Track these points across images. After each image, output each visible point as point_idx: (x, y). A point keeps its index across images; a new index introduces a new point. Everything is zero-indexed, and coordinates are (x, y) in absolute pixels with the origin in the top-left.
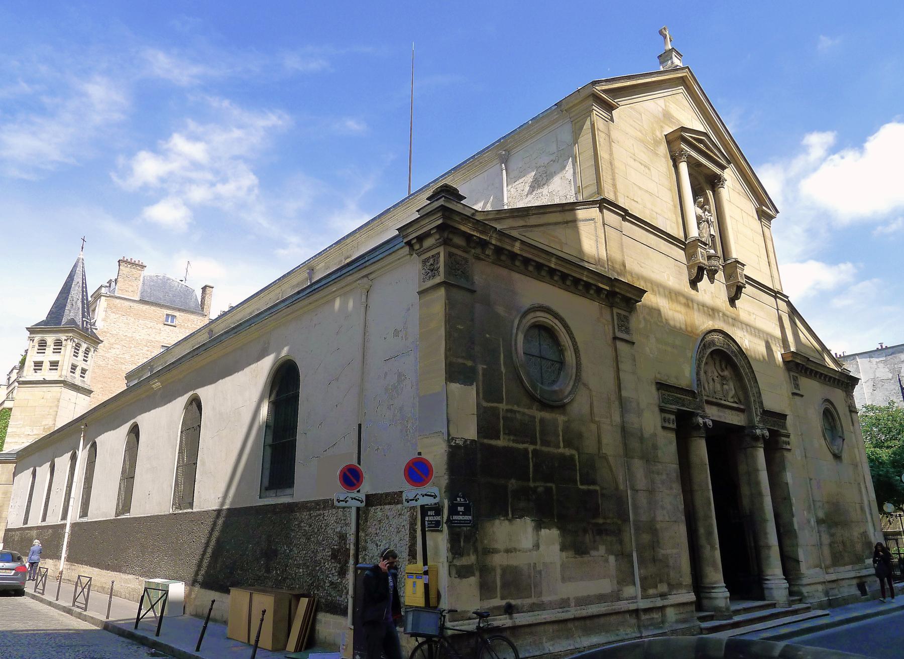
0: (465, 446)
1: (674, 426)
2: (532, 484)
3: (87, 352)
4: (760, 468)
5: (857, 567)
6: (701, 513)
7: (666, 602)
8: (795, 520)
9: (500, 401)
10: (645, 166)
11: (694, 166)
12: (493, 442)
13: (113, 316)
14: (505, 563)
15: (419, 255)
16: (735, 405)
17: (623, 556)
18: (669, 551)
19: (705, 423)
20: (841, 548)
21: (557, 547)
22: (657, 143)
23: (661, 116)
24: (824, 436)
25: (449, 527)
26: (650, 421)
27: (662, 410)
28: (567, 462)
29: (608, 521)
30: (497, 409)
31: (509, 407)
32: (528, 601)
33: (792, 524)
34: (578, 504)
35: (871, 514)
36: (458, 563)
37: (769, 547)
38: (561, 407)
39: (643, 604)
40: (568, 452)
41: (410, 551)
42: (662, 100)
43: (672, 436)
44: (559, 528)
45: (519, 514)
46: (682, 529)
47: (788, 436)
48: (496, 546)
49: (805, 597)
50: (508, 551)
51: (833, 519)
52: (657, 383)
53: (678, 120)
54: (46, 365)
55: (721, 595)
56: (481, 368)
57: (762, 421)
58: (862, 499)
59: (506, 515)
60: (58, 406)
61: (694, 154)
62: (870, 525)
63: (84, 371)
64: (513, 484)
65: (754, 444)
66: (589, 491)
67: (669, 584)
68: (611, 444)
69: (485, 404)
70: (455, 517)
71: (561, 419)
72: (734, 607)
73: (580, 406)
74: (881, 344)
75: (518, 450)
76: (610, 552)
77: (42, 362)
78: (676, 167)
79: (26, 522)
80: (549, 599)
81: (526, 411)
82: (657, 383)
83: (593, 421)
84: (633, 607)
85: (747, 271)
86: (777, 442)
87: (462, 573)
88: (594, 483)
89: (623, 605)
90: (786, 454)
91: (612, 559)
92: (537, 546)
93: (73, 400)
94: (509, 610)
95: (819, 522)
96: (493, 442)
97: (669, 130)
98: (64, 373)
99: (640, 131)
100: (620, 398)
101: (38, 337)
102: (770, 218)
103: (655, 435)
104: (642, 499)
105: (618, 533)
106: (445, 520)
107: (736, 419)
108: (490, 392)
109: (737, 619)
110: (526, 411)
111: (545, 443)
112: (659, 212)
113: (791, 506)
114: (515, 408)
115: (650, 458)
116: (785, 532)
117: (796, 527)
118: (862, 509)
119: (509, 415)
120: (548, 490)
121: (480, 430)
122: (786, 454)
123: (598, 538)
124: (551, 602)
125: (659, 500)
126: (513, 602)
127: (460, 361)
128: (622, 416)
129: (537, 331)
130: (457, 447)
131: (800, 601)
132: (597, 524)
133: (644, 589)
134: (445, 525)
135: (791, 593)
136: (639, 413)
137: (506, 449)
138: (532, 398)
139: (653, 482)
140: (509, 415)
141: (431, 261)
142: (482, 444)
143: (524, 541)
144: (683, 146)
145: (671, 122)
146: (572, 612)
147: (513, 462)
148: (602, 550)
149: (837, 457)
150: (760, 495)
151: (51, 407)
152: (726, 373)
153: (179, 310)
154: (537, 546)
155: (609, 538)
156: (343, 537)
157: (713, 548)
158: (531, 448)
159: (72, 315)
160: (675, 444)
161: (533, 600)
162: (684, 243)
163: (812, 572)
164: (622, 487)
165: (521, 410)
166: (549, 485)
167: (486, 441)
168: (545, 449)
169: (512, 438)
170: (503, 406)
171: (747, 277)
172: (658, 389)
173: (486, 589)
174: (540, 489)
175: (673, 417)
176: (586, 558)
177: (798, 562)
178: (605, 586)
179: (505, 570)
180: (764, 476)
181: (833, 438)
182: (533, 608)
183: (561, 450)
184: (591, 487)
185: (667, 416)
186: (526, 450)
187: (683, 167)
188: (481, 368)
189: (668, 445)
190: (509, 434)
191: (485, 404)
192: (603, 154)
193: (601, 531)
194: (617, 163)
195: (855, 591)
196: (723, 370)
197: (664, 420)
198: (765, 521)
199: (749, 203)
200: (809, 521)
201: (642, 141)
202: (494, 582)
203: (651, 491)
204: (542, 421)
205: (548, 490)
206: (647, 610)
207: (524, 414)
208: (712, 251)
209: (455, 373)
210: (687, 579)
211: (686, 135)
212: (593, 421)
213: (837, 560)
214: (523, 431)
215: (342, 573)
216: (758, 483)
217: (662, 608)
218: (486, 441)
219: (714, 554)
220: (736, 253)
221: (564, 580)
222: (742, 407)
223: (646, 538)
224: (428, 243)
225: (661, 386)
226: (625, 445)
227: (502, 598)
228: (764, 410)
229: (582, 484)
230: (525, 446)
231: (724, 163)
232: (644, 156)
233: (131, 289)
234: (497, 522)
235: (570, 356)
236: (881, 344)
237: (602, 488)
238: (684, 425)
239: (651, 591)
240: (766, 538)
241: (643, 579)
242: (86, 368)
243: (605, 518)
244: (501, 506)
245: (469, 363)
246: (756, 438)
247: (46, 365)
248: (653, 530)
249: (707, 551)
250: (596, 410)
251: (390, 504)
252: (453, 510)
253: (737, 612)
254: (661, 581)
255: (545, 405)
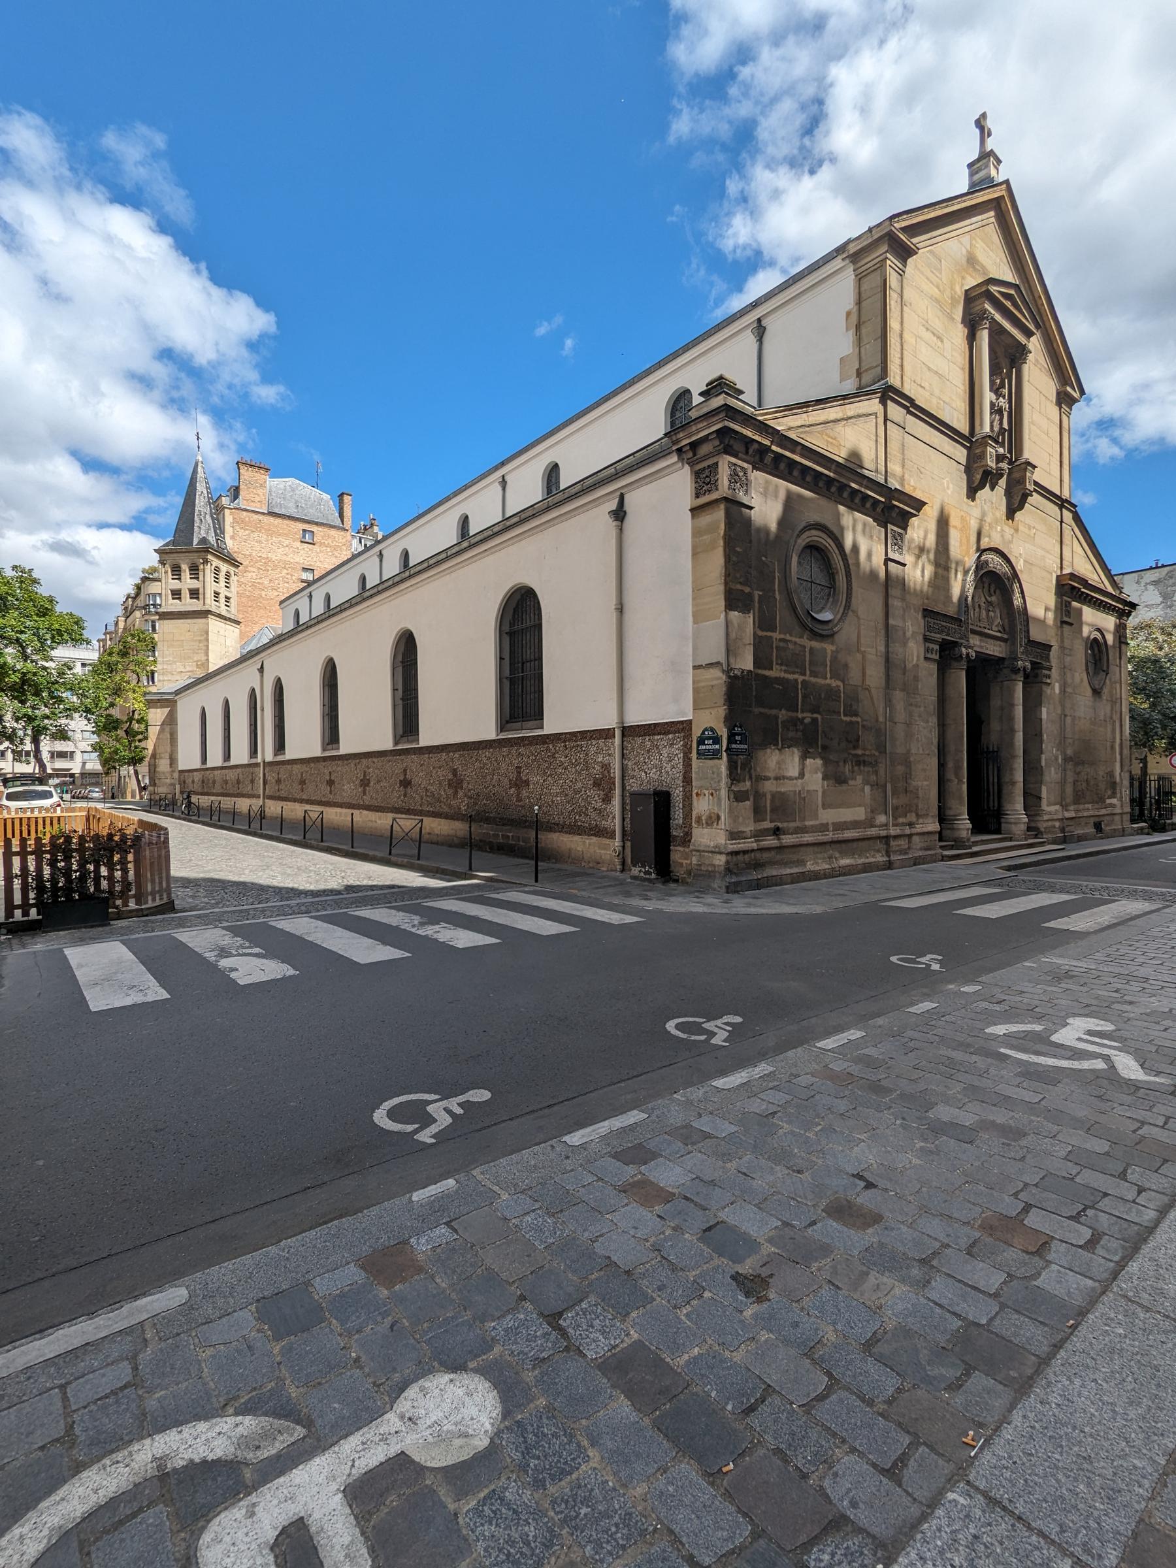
0: (743, 677)
1: (937, 657)
2: (800, 715)
3: (228, 576)
4: (1016, 702)
5: (1096, 806)
6: (952, 747)
7: (914, 831)
8: (1043, 756)
9: (774, 630)
10: (938, 337)
11: (997, 332)
12: (767, 673)
13: (241, 532)
14: (774, 789)
15: (691, 464)
16: (999, 635)
17: (879, 786)
18: (920, 783)
19: (968, 654)
20: (1084, 784)
21: (820, 775)
22: (954, 300)
23: (964, 261)
24: (1087, 669)
25: (728, 755)
26: (914, 650)
27: (926, 639)
28: (832, 694)
29: (867, 752)
30: (771, 637)
31: (782, 636)
32: (792, 825)
33: (1039, 760)
34: (839, 735)
35: (1121, 754)
36: (733, 788)
37: (1013, 783)
38: (829, 637)
39: (893, 831)
40: (835, 683)
41: (684, 777)
42: (967, 237)
43: (933, 667)
44: (822, 758)
45: (789, 744)
46: (934, 761)
47: (1050, 669)
48: (767, 774)
49: (1042, 833)
50: (777, 778)
51: (1081, 757)
52: (925, 610)
53: (983, 267)
54: (185, 594)
55: (964, 824)
56: (757, 593)
57: (1025, 652)
58: (1114, 738)
59: (777, 745)
60: (207, 640)
61: (998, 317)
62: (1118, 765)
63: (227, 598)
64: (783, 715)
65: (1014, 677)
66: (851, 722)
67: (917, 815)
68: (875, 676)
69: (760, 633)
70: (734, 746)
71: (829, 648)
72: (973, 839)
73: (847, 632)
74: (1157, 561)
75: (787, 680)
76: (866, 782)
77: (180, 590)
78: (972, 338)
79: (204, 759)
80: (811, 823)
81: (797, 640)
82: (925, 610)
83: (858, 651)
84: (883, 833)
85: (1037, 476)
86: (1036, 676)
87: (739, 797)
88: (856, 715)
89: (873, 832)
90: (1044, 688)
91: (867, 789)
92: (802, 775)
93: (222, 632)
94: (777, 832)
95: (1066, 759)
96: (767, 673)
97: (971, 282)
98: (208, 601)
99: (938, 287)
100: (887, 625)
101: (170, 559)
102: (1071, 401)
103: (917, 666)
104: (900, 731)
105: (874, 764)
106: (724, 748)
107: (995, 649)
108: (765, 623)
109: (975, 849)
110: (797, 640)
111: (814, 674)
112: (947, 400)
113: (1041, 742)
114: (788, 637)
115: (910, 689)
116: (1033, 769)
117: (1043, 764)
118: (1113, 747)
119: (782, 644)
120: (815, 720)
121: (757, 663)
122: (1044, 688)
123: (856, 768)
124: (812, 826)
125: (919, 736)
126: (780, 825)
127: (739, 587)
128: (887, 646)
129: (808, 551)
130: (736, 677)
131: (1036, 836)
132: (857, 755)
133: (895, 818)
134: (724, 754)
135: (1029, 829)
136: (905, 644)
137: (778, 680)
138: (804, 626)
139: (911, 715)
140: (782, 644)
141: (707, 472)
142: (757, 675)
143: (791, 769)
144: (988, 306)
145: (975, 269)
146: (830, 836)
147: (786, 694)
148: (859, 779)
149: (1096, 692)
150: (1012, 731)
151: (200, 641)
152: (993, 599)
153: (317, 524)
154: (802, 775)
155: (866, 769)
156: (606, 767)
157: (960, 781)
158: (801, 678)
159: (203, 534)
160: (935, 676)
161: (798, 824)
162: (971, 442)
163: (1052, 808)
164: (881, 719)
165: (794, 639)
166: (815, 715)
167: (760, 671)
168: (813, 680)
169: (784, 668)
170: (776, 635)
171: (1036, 483)
172: (924, 617)
173: (758, 813)
174: (807, 721)
175: (936, 647)
176: (844, 787)
177: (1040, 798)
178: (859, 813)
179: (774, 796)
180: (1019, 711)
181: (1096, 673)
182: (797, 831)
183: (828, 681)
184: (854, 719)
185: (931, 646)
186: (796, 680)
187: (984, 336)
188: (757, 593)
189: (928, 674)
190: (781, 665)
191: (760, 633)
192: (893, 324)
193: (860, 762)
194: (906, 336)
195: (1091, 830)
196: (990, 595)
197: (927, 650)
198: (1014, 757)
199: (1051, 381)
200: (1056, 759)
201: (937, 301)
202: (765, 806)
203: (908, 725)
204: (811, 649)
205: (815, 720)
206: (896, 837)
207: (795, 643)
208: (1001, 451)
209: (733, 600)
210: (935, 811)
211: (994, 289)
212: (858, 651)
213: (1078, 798)
214: (794, 662)
215: (607, 799)
216: (1011, 719)
217: (910, 836)
218: (760, 671)
219: (961, 787)
220: (1029, 452)
221: (824, 806)
222: (1006, 636)
223: (900, 769)
224: (704, 450)
225: (927, 613)
226: (888, 676)
227: (771, 822)
228: (1029, 641)
229: (845, 715)
230: (796, 676)
231: (1032, 327)
232: (938, 324)
233: (257, 499)
234: (769, 751)
235: (841, 578)
236: (1157, 561)
237: (863, 720)
238: (946, 654)
239: (901, 820)
240: (1012, 774)
241: (895, 809)
242: (229, 595)
243: (864, 749)
244: (771, 737)
245: (747, 590)
246: (1016, 671)
247: (185, 594)
248: (907, 763)
249: (953, 785)
250: (862, 641)
251: (659, 734)
252: (731, 739)
253: (976, 843)
254: (911, 811)
255: (816, 635)
